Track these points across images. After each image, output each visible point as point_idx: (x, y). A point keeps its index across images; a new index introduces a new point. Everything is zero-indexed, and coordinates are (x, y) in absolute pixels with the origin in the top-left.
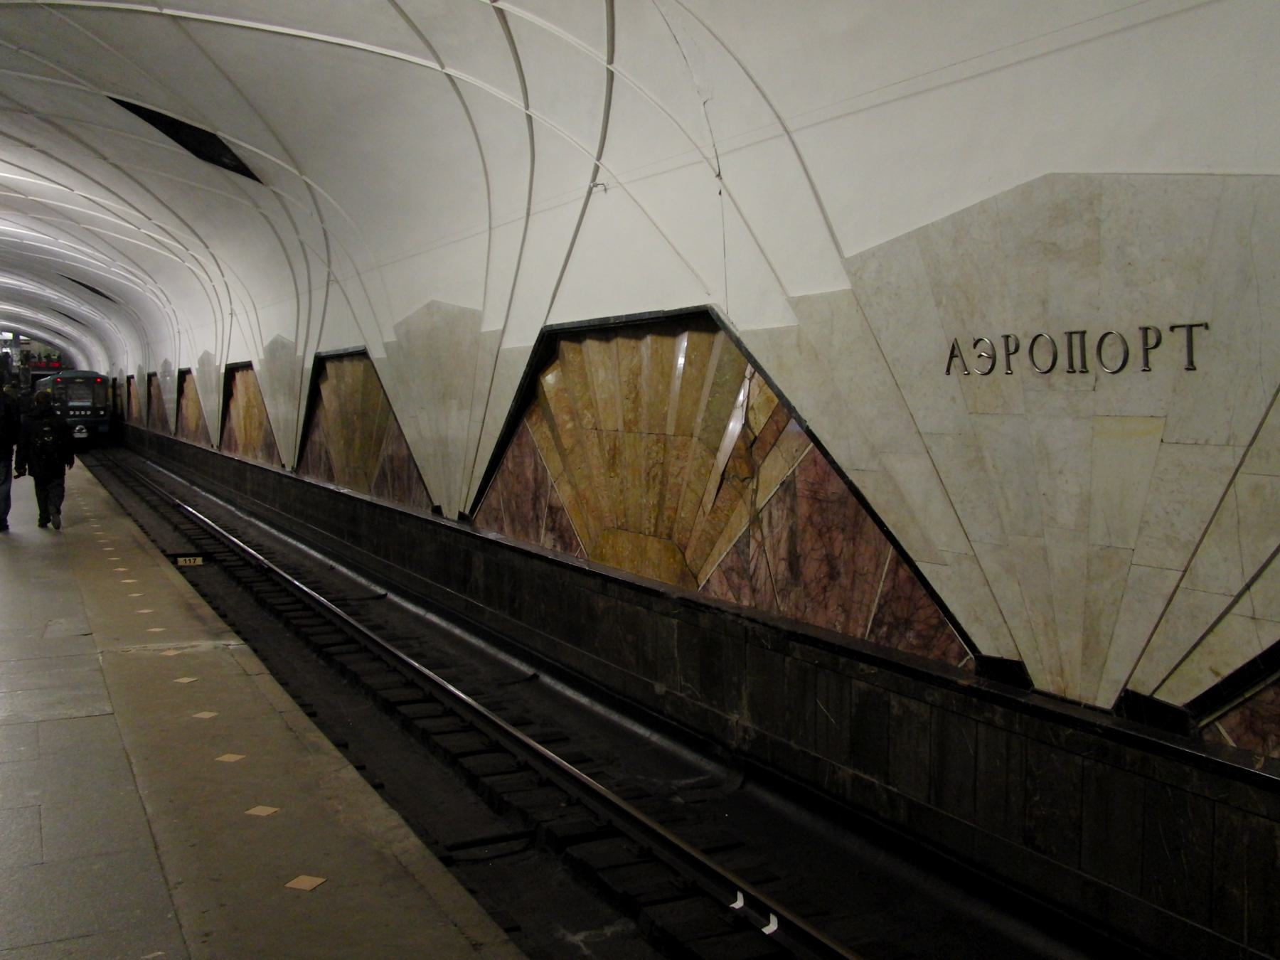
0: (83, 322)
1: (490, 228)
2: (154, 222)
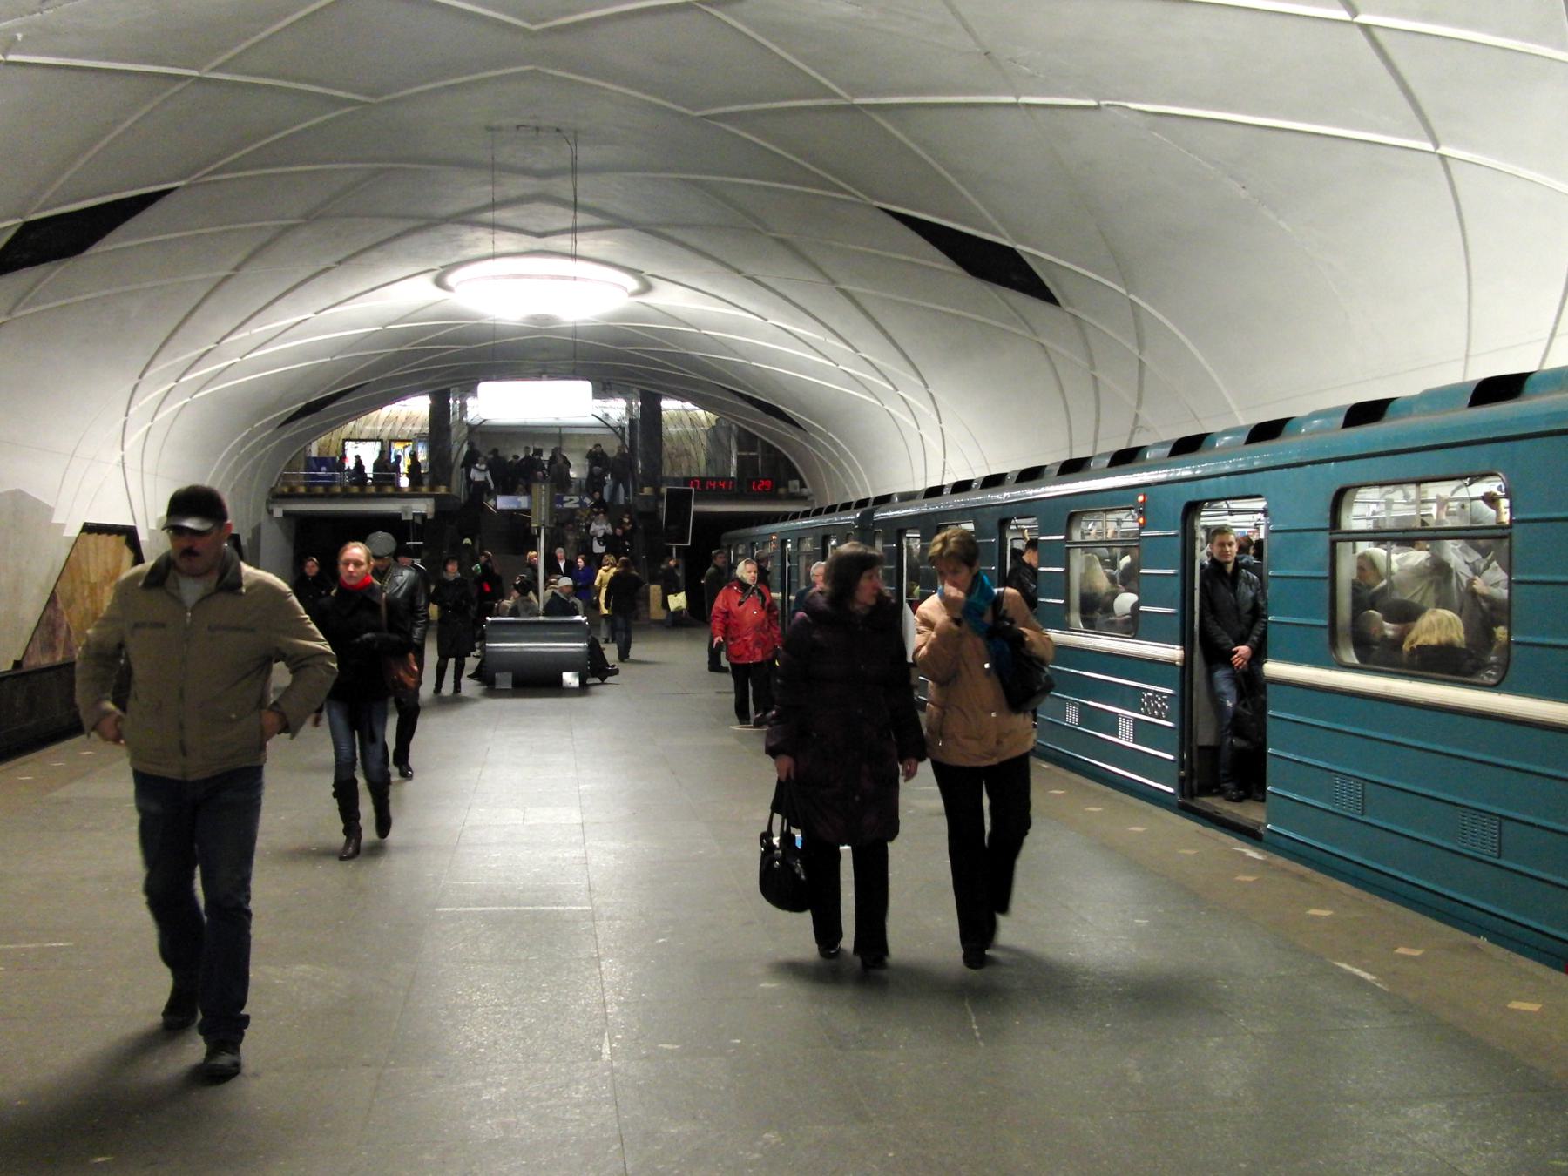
1: (1467, 356)
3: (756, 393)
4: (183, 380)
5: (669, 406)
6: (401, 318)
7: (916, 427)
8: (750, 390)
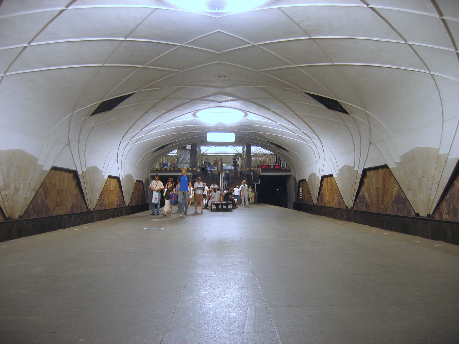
0: (288, 151)
1: (443, 121)
2: (302, 131)
3: (277, 143)
4: (131, 140)
5: (254, 149)
6: (184, 124)
7: (317, 150)
8: (276, 143)
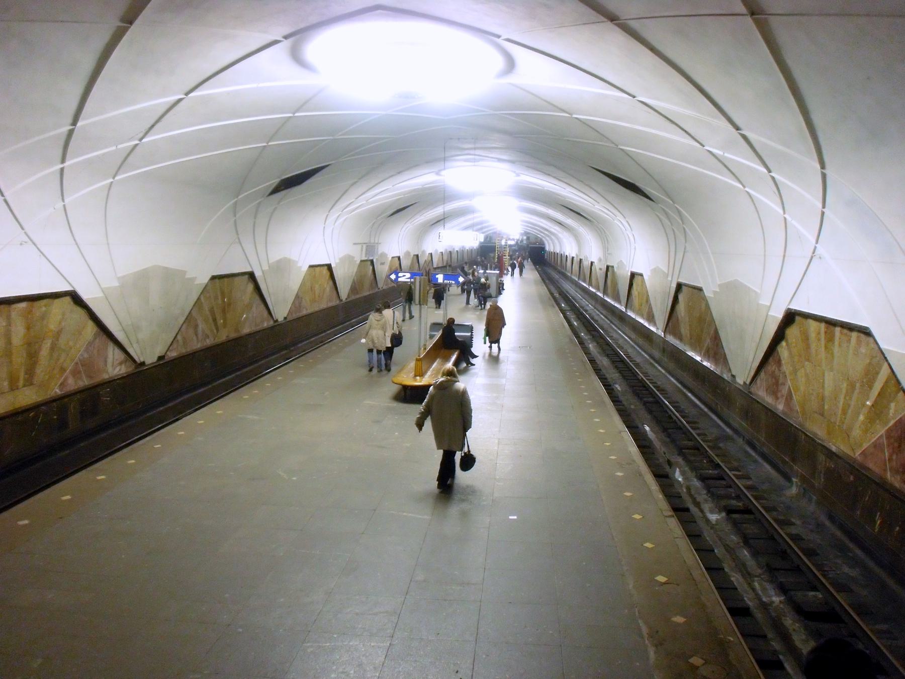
0: (589, 217)
4: (344, 211)
